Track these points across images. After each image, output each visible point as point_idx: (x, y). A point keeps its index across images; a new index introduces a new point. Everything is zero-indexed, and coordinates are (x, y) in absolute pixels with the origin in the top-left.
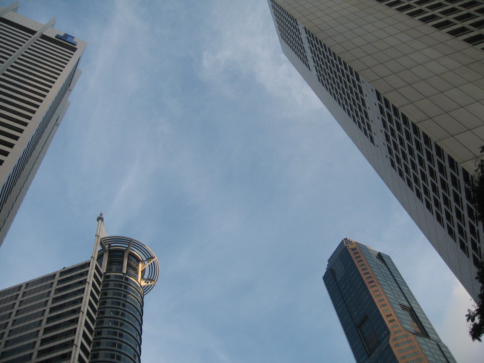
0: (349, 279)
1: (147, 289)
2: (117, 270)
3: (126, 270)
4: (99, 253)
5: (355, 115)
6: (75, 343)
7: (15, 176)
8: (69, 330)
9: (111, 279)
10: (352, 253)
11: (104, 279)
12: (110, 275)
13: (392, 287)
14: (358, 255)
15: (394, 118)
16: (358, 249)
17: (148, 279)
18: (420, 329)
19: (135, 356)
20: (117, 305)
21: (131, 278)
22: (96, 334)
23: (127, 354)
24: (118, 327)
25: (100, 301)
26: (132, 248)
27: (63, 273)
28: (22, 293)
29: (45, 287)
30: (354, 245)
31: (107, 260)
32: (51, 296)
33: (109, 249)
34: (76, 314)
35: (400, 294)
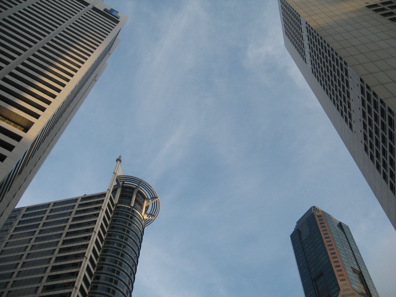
0: (312, 240)
1: (148, 222)
3: (136, 198)
4: (115, 187)
5: (335, 99)
6: (86, 255)
10: (317, 219)
11: (115, 208)
13: (347, 252)
14: (322, 222)
15: (374, 122)
16: (322, 216)
18: (366, 290)
20: (123, 231)
21: (137, 212)
23: (123, 280)
24: (121, 248)
25: (103, 249)
26: (140, 187)
27: (83, 199)
29: (47, 253)
30: (320, 213)
31: (119, 194)
33: (122, 185)
34: (90, 233)
35: (353, 259)
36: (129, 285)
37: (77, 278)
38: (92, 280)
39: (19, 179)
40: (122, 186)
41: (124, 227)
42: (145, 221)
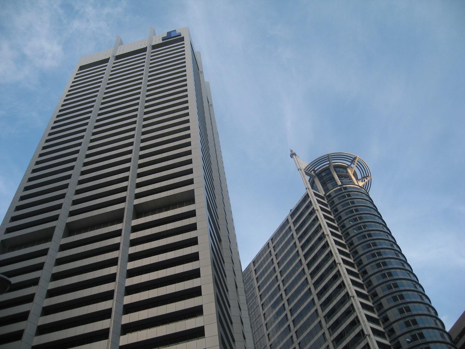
1: (368, 186)
2: (333, 186)
3: (337, 174)
4: (310, 181)
6: (337, 262)
7: (210, 178)
8: (342, 297)
9: (333, 196)
12: (330, 194)
17: (363, 178)
19: (403, 265)
22: (338, 221)
24: (363, 230)
25: (343, 235)
26: (333, 161)
27: (292, 215)
28: (279, 273)
29: (286, 233)
32: (292, 229)
36: (404, 266)
37: (346, 287)
38: (344, 240)
39: (224, 244)
40: (315, 175)
41: (350, 210)
42: (364, 188)
